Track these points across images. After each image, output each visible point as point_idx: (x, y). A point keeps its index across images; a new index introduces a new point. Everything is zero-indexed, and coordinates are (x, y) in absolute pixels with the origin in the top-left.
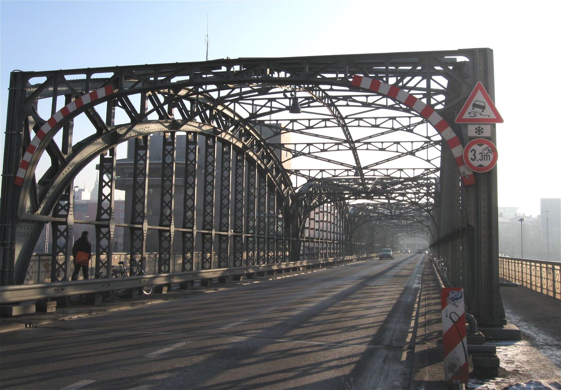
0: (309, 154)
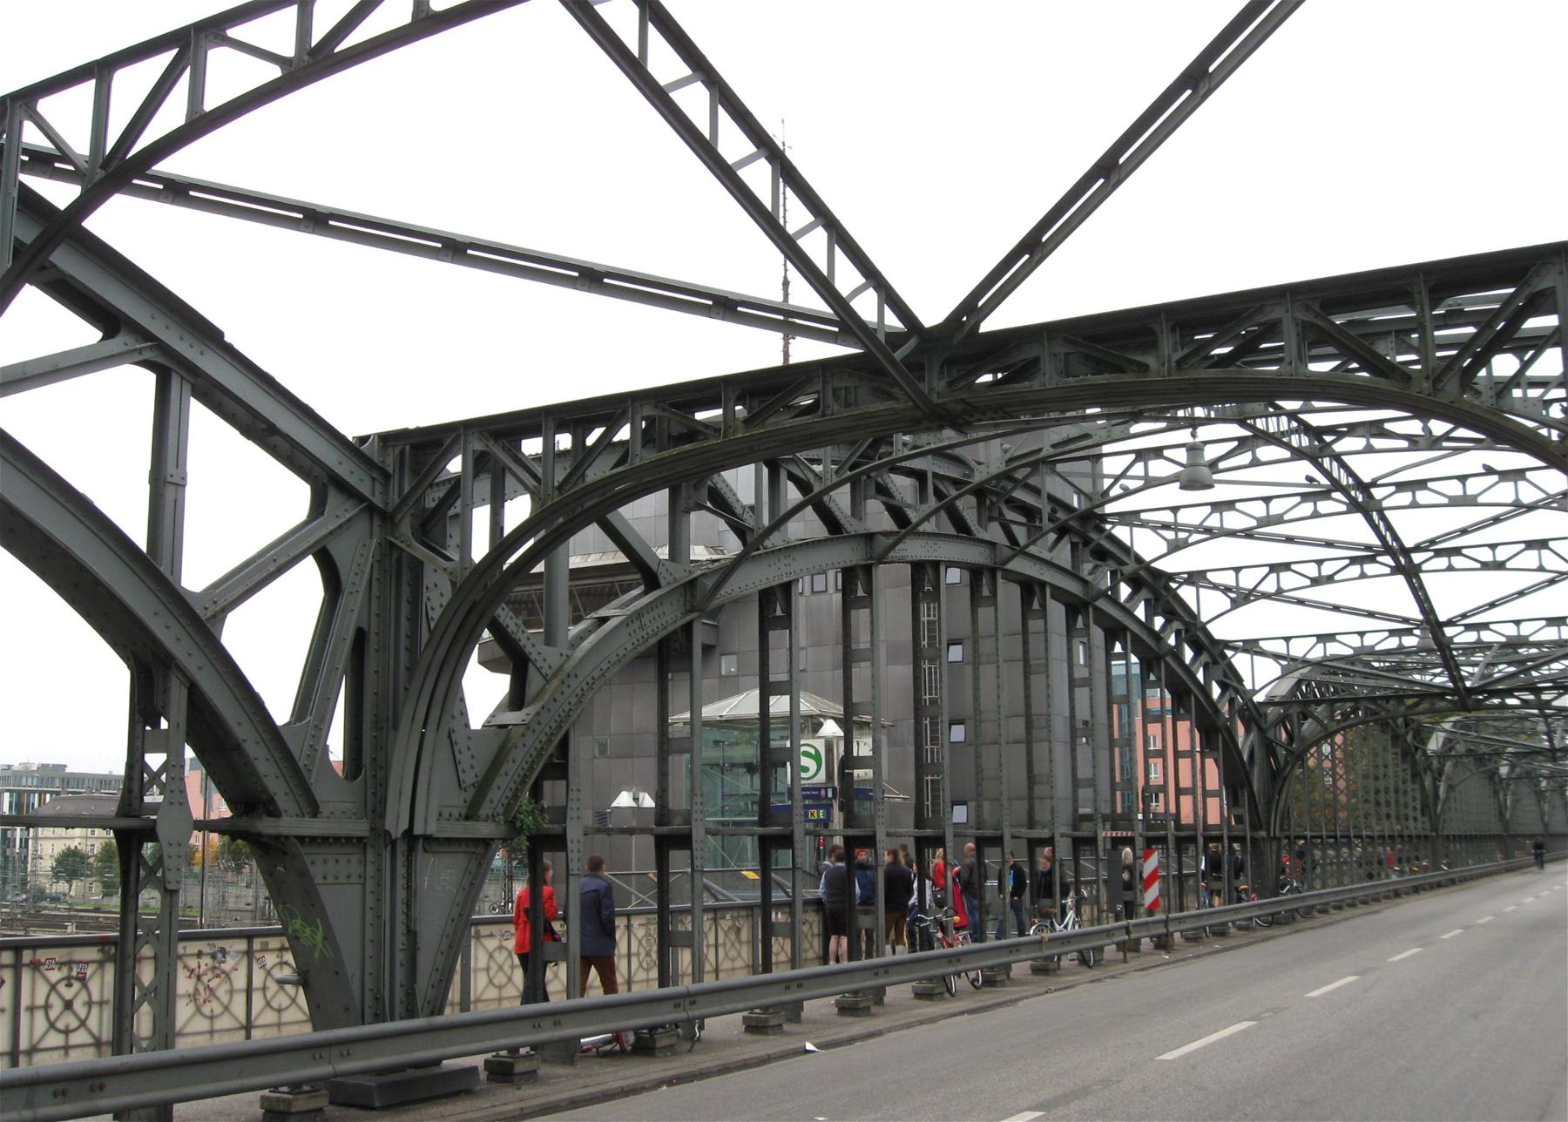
0: (1279, 595)
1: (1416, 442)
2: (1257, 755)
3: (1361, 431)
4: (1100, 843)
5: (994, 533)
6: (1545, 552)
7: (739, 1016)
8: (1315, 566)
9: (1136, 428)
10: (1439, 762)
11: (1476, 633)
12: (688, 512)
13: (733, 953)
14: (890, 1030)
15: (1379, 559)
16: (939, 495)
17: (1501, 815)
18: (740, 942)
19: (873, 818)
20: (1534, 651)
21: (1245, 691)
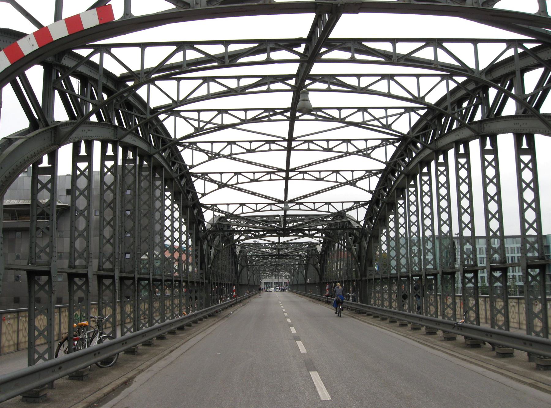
0: (230, 157)
13: (9, 338)
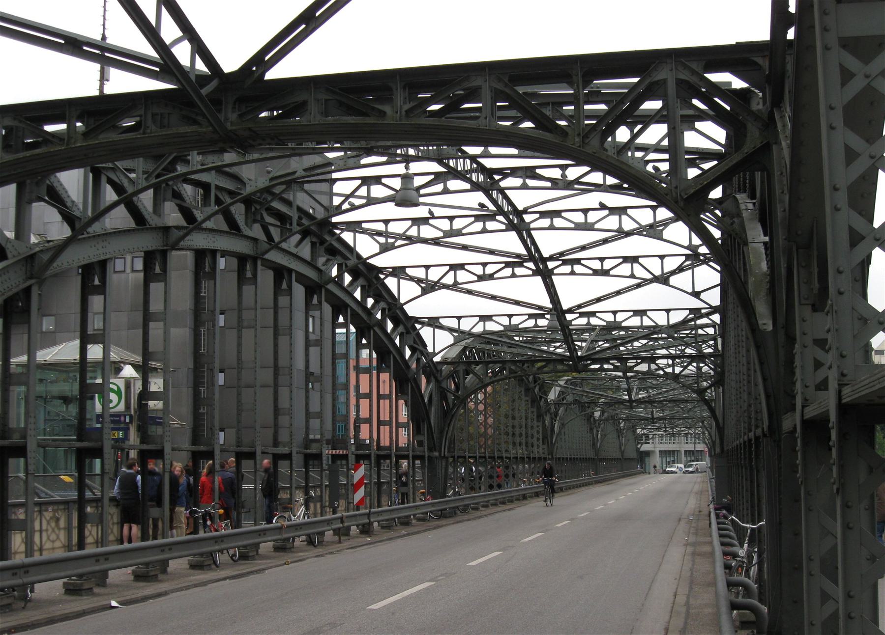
0: (455, 287)
1: (557, 183)
2: (435, 398)
3: (520, 173)
4: (324, 458)
5: (256, 231)
6: (636, 265)
7: (60, 582)
8: (480, 267)
9: (364, 161)
10: (555, 408)
11: (586, 319)
12: (30, 202)
13: (53, 537)
14: (173, 591)
15: (525, 264)
16: (218, 202)
17: (594, 444)
18: (59, 529)
19: (162, 437)
20: (622, 333)
21: (428, 353)
